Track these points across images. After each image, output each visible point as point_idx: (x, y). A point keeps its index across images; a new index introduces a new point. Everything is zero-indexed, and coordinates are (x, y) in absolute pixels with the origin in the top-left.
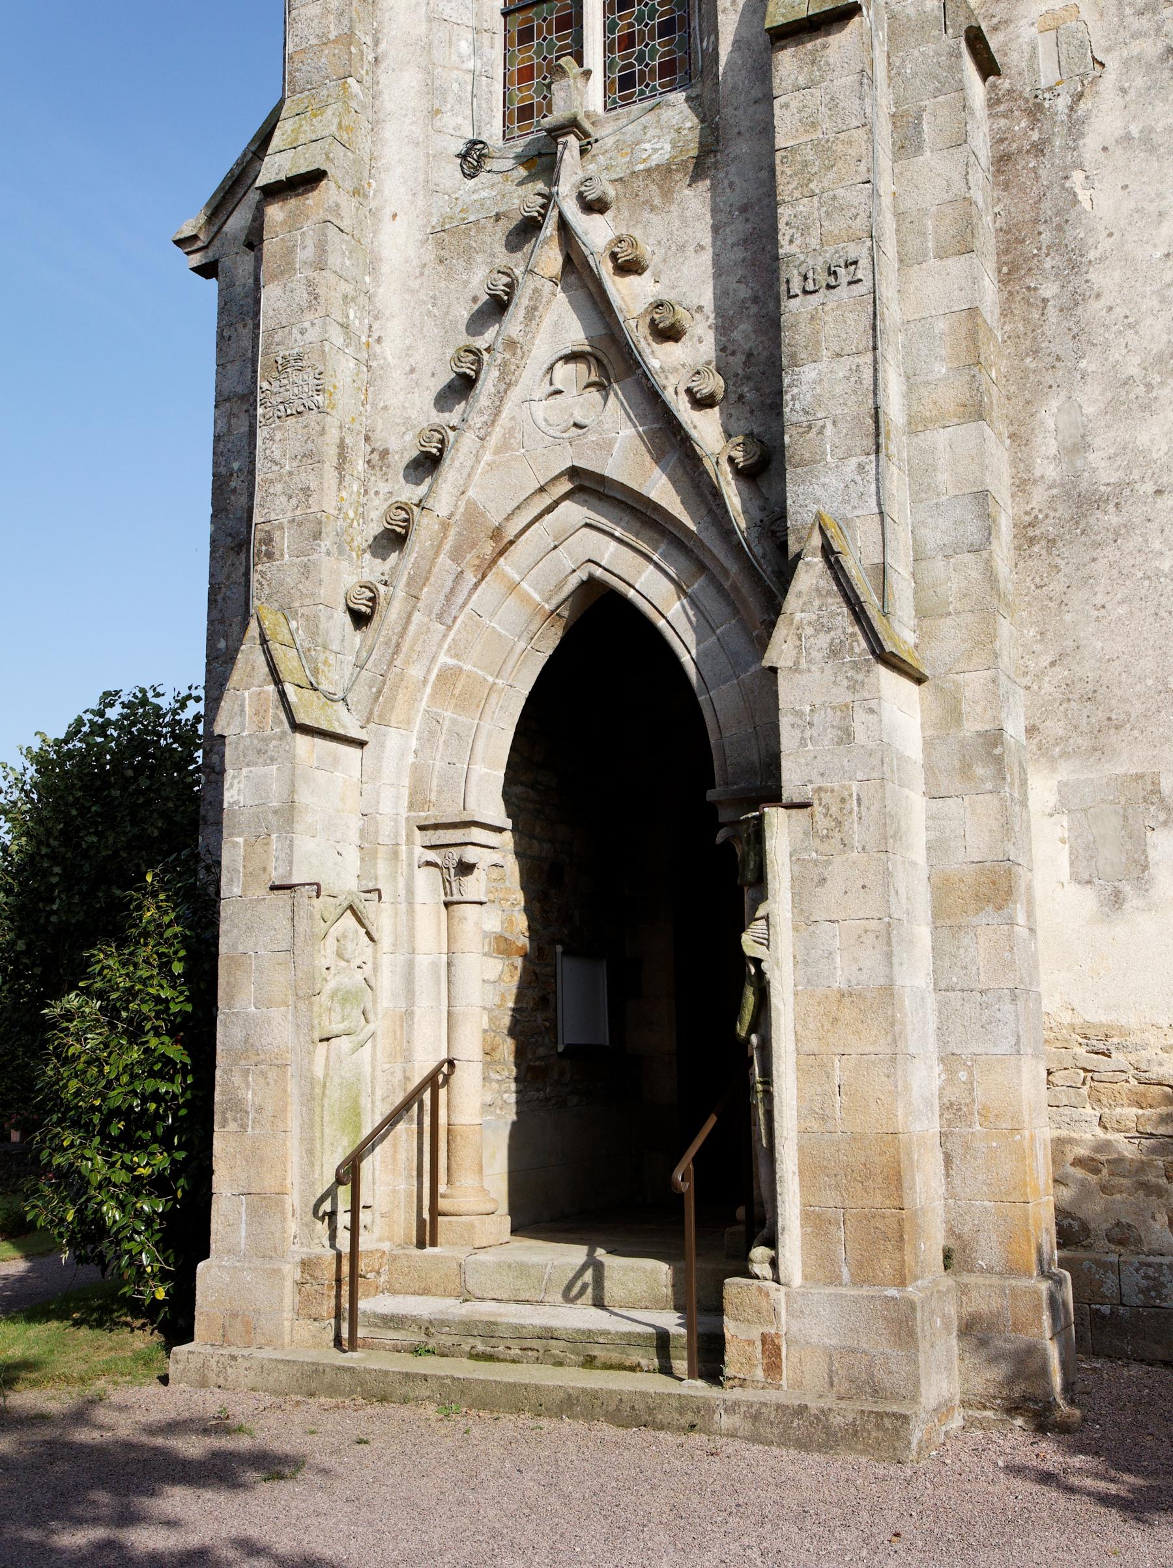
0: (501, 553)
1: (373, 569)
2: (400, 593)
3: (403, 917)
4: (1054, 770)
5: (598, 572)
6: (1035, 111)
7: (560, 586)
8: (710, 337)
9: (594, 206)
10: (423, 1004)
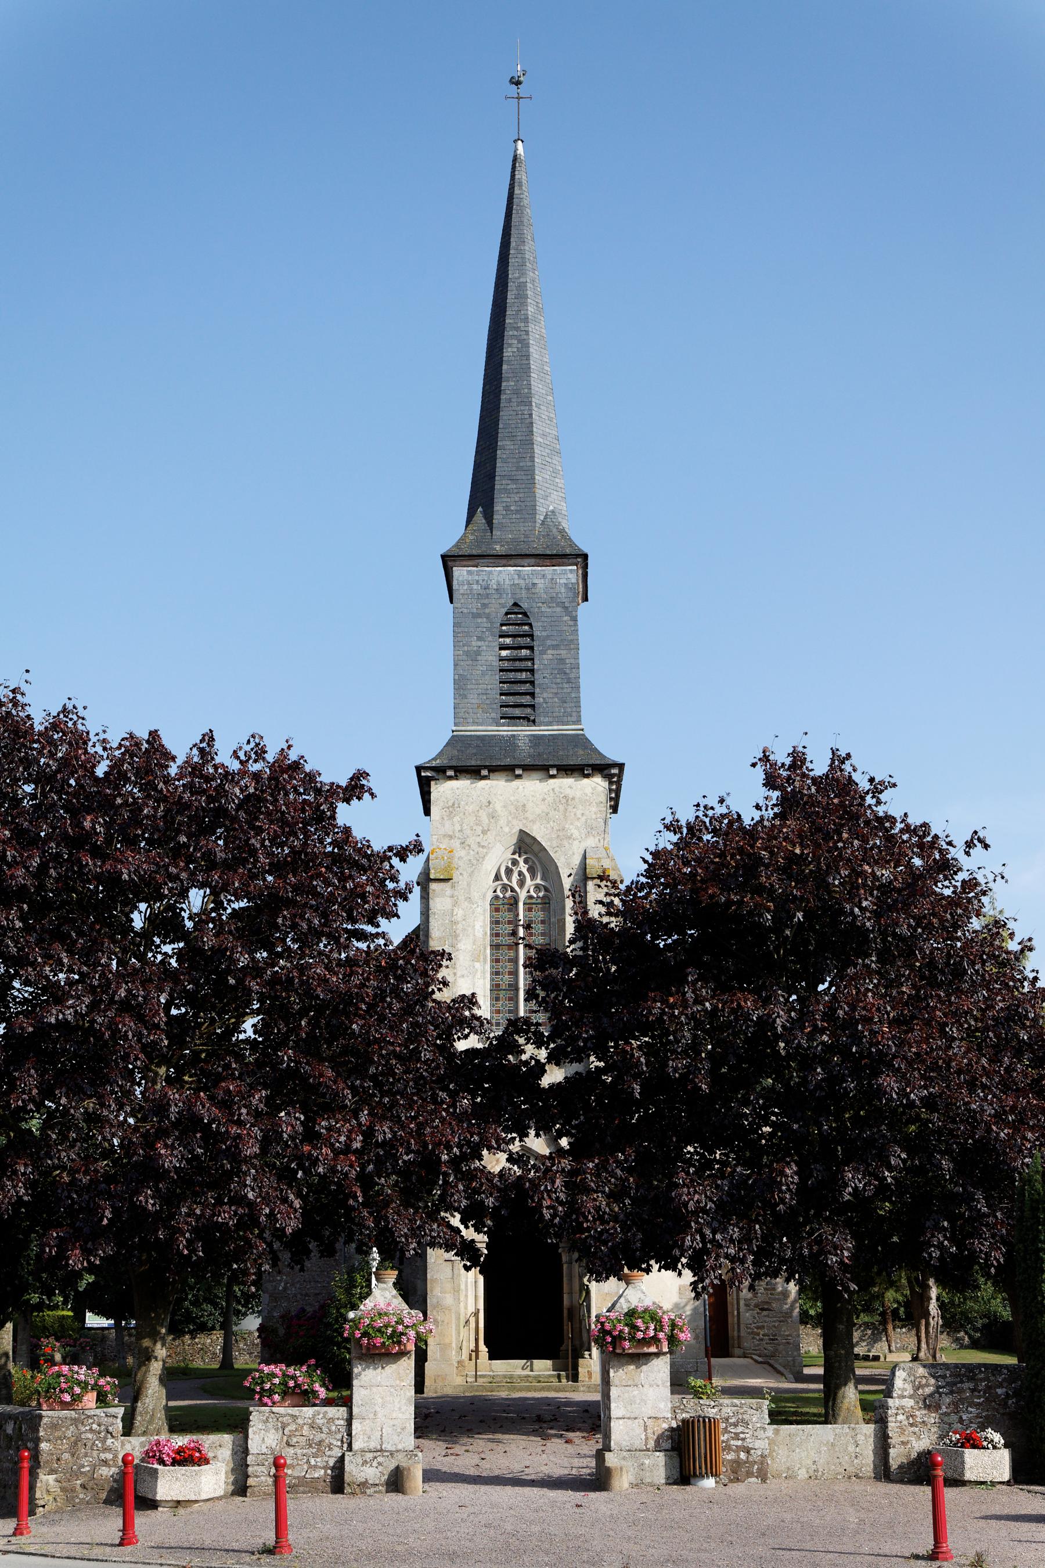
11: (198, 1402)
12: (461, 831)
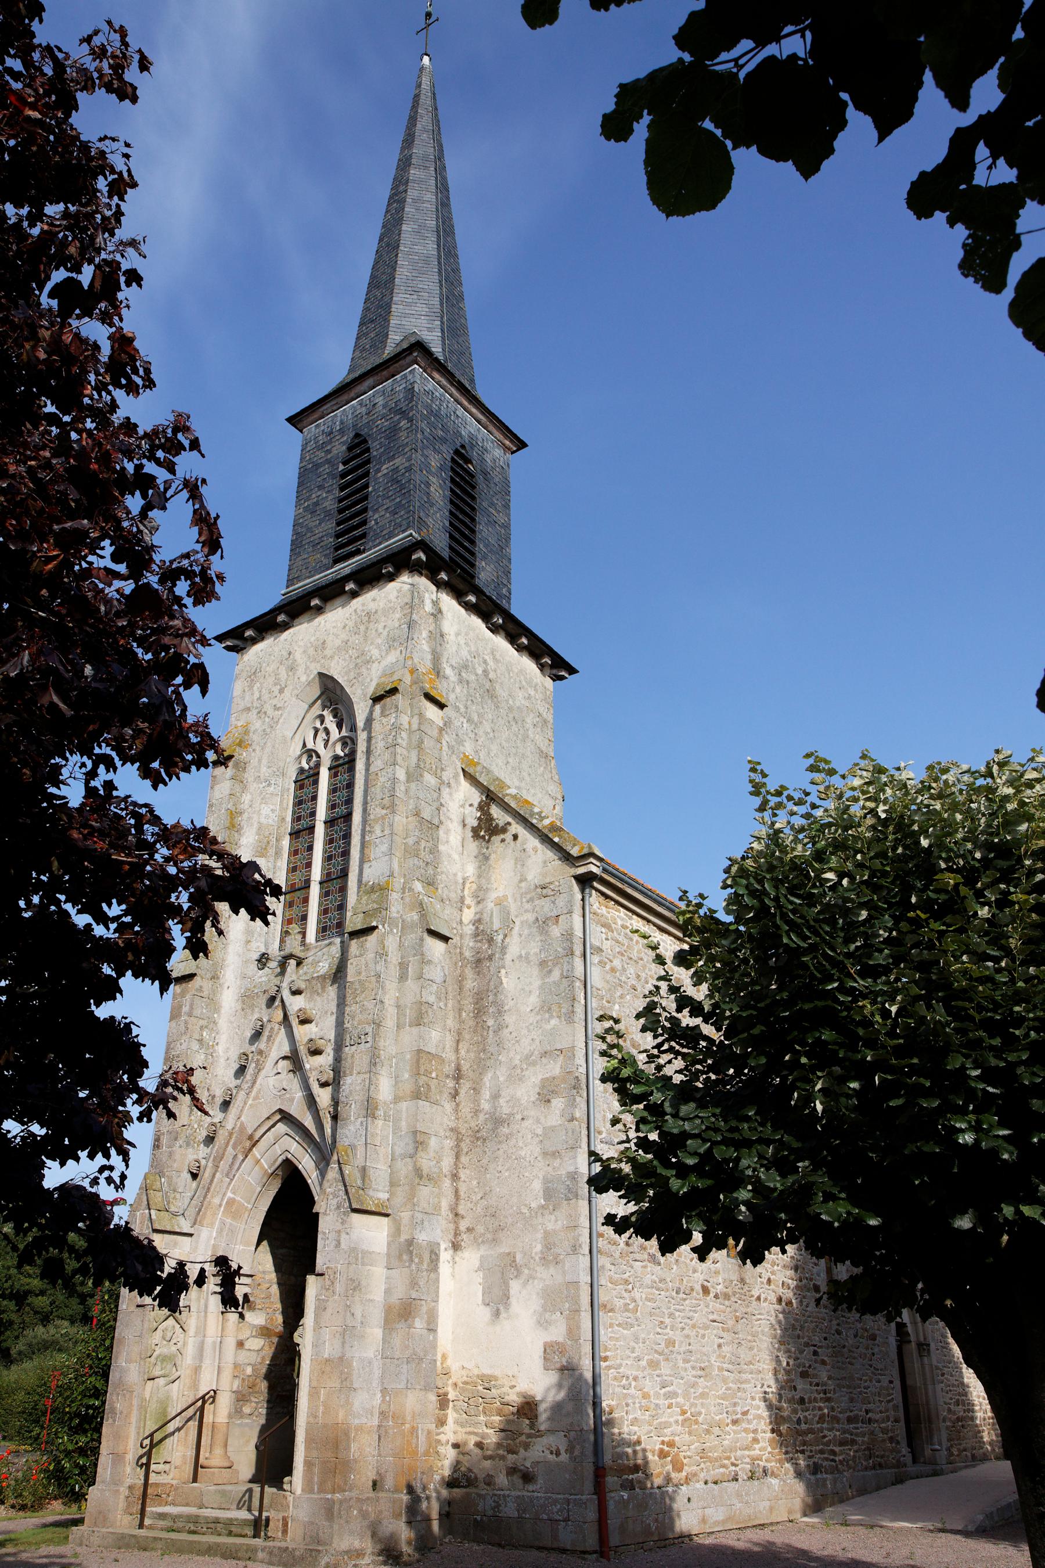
0: (254, 1146)
1: (203, 1151)
2: (210, 1164)
3: (202, 1319)
4: (479, 1249)
5: (289, 1156)
6: (491, 941)
7: (276, 1160)
8: (332, 1053)
9: (296, 992)
10: (207, 1363)
11: (61, 705)
12: (259, 699)
